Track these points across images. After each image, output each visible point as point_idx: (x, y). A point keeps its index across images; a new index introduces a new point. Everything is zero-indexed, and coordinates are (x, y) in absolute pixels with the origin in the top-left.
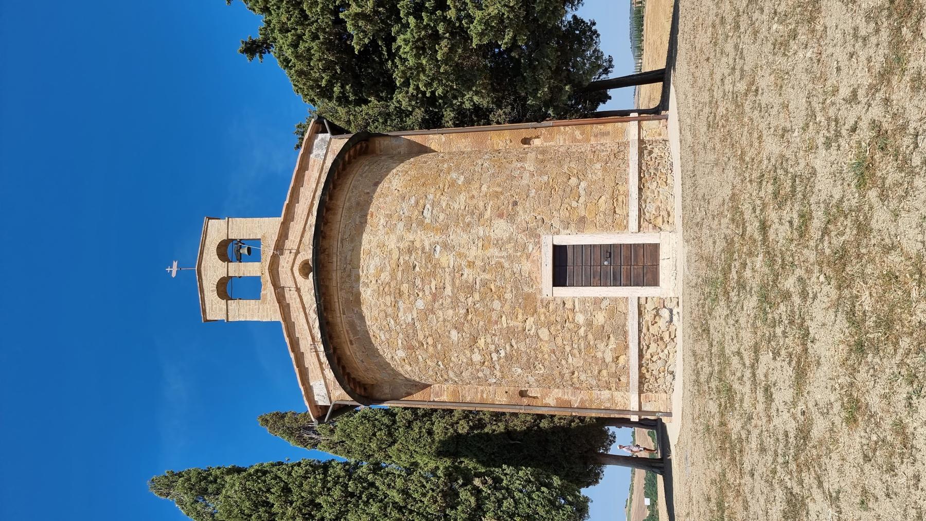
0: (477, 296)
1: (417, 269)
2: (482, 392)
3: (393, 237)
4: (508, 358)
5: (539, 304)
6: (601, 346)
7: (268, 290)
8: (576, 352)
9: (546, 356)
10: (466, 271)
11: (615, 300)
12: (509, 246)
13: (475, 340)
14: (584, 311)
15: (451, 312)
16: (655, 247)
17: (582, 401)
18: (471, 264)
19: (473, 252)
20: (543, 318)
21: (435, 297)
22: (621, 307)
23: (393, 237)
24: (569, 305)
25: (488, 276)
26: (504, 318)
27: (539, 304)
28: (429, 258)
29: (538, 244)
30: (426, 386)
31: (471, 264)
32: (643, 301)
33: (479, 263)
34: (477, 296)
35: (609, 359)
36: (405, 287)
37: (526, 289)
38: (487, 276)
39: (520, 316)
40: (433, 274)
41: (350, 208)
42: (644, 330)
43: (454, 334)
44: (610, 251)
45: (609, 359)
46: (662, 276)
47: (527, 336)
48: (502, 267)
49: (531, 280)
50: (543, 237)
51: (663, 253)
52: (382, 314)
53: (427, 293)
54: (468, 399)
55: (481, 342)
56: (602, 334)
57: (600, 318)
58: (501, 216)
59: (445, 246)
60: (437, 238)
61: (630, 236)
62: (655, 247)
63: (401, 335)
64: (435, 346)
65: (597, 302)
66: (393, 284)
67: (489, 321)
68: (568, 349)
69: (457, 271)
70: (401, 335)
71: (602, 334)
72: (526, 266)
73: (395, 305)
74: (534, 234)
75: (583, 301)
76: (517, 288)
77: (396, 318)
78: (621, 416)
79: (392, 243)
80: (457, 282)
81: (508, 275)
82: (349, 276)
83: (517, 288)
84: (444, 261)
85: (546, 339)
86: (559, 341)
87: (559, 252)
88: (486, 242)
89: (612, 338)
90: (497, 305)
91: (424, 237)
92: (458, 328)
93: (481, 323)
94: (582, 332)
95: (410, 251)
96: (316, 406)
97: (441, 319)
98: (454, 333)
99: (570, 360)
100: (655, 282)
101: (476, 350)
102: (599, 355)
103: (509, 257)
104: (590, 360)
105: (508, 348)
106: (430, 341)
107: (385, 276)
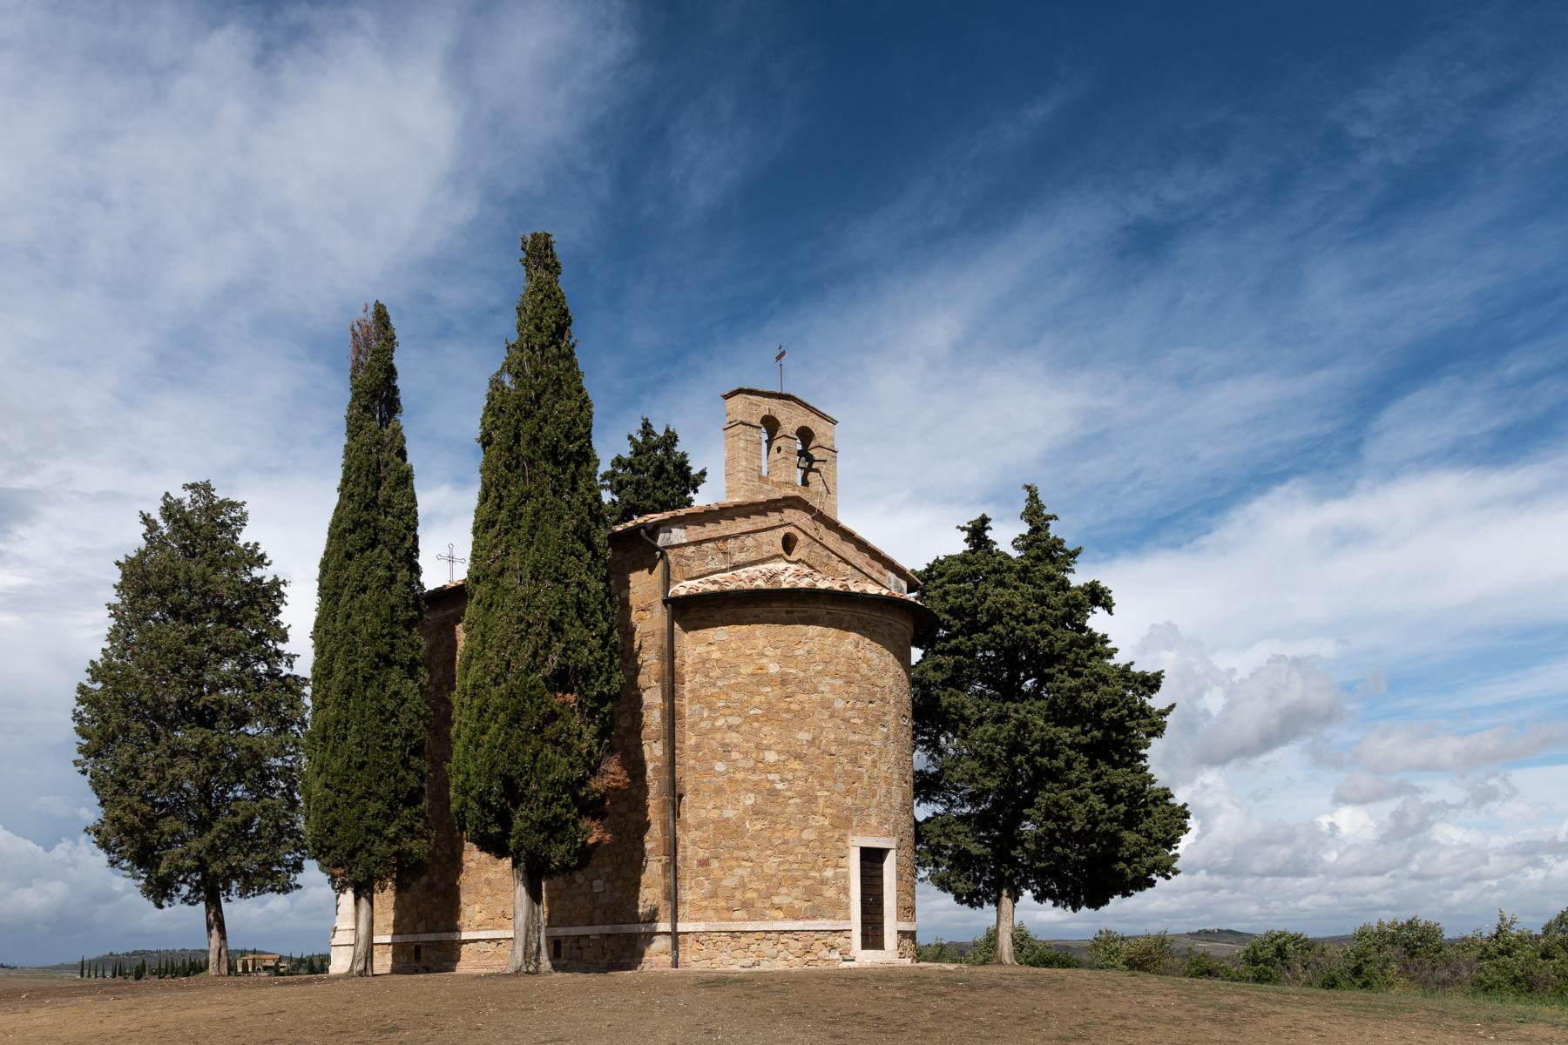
0: (848, 767)
4: (773, 793)
6: (797, 892)
11: (847, 908)
14: (836, 877)
21: (846, 720)
22: (841, 914)
24: (842, 862)
31: (874, 762)
34: (848, 767)
35: (776, 900)
36: (855, 689)
40: (866, 723)
43: (804, 736)
49: (864, 828)
55: (795, 765)
57: (830, 893)
64: (788, 711)
65: (845, 890)
67: (823, 777)
71: (811, 893)
73: (836, 675)
75: (846, 877)
86: (803, 849)
90: (841, 787)
92: (812, 743)
94: (813, 874)
100: (864, 947)
102: (784, 890)
103: (880, 804)
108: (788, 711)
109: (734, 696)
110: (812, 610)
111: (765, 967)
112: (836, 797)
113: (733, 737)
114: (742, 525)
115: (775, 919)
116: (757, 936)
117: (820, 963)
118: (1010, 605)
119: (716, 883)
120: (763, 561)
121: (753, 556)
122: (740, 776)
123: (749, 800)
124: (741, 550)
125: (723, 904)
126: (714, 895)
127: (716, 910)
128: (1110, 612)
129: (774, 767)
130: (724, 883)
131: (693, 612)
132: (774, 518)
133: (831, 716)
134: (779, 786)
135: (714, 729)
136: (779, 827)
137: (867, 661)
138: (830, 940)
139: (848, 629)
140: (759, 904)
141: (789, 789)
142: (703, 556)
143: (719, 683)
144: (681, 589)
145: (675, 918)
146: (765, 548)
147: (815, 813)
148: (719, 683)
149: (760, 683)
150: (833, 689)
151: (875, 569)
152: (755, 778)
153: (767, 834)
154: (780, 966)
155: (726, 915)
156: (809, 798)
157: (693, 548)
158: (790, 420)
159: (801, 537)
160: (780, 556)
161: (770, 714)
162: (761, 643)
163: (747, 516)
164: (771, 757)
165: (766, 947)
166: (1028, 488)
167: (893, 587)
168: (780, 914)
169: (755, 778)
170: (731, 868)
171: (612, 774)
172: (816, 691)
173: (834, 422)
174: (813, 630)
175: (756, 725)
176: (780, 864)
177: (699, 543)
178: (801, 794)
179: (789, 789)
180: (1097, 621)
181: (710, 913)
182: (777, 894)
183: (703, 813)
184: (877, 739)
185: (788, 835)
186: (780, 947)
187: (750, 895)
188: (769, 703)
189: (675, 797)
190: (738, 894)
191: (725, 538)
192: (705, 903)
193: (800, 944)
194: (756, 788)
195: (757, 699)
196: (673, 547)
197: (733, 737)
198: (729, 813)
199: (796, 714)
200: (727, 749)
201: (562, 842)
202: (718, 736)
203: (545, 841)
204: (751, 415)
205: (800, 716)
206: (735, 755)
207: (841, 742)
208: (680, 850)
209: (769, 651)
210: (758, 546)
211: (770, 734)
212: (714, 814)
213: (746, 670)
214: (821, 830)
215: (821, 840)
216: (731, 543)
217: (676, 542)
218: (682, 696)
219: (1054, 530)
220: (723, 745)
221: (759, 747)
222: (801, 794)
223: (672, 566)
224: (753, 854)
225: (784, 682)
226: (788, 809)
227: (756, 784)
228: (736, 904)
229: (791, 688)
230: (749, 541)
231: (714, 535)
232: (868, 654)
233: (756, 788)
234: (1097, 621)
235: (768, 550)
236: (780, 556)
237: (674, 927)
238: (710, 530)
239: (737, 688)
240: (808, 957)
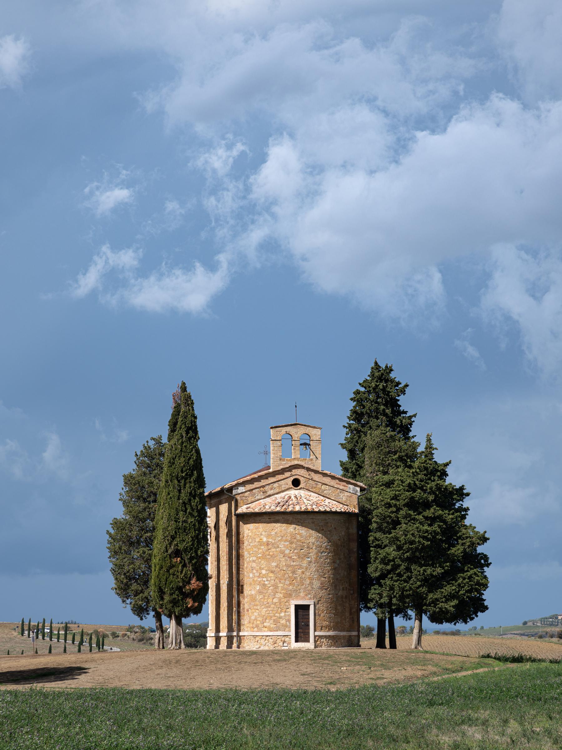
0: (291, 575)
4: (264, 585)
6: (272, 621)
11: (290, 627)
13: (272, 572)
15: (284, 564)
16: (309, 641)
22: (287, 629)
24: (288, 610)
29: (311, 599)
30: (301, 444)
31: (303, 573)
32: (289, 637)
34: (291, 575)
35: (265, 624)
40: (299, 558)
41: (326, 520)
43: (274, 564)
45: (265, 624)
46: (299, 643)
49: (297, 597)
53: (292, 555)
57: (283, 622)
62: (309, 641)
63: (273, 541)
64: (269, 555)
65: (289, 621)
66: (295, 540)
68: (269, 609)
70: (273, 541)
71: (276, 622)
72: (302, 594)
73: (286, 541)
75: (289, 616)
78: (211, 531)
82: (298, 522)
83: (294, 591)
86: (273, 606)
87: (307, 607)
91: (314, 553)
92: (276, 566)
94: (276, 615)
100: (297, 641)
101: (267, 572)
102: (267, 621)
103: (306, 588)
105: (269, 585)
108: (269, 555)
110: (277, 517)
111: (262, 648)
112: (286, 586)
113: (254, 565)
114: (271, 480)
115: (265, 631)
117: (279, 647)
120: (283, 491)
121: (277, 491)
122: (255, 579)
123: (258, 588)
124: (271, 489)
129: (265, 576)
132: (287, 474)
133: (284, 556)
134: (266, 583)
136: (266, 598)
137: (300, 534)
139: (291, 524)
141: (269, 584)
145: (239, 630)
146: (283, 486)
149: (261, 545)
150: (285, 547)
152: (259, 580)
153: (262, 600)
154: (266, 648)
155: (252, 629)
156: (276, 587)
157: (249, 493)
159: (301, 479)
160: (291, 488)
161: (264, 557)
162: (261, 530)
163: (267, 478)
164: (264, 572)
165: (262, 641)
168: (266, 629)
169: (259, 580)
170: (253, 613)
171: (194, 584)
172: (278, 547)
174: (278, 525)
175: (260, 560)
177: (251, 490)
178: (273, 586)
179: (269, 584)
184: (305, 564)
186: (266, 641)
187: (258, 622)
190: (255, 622)
191: (263, 487)
193: (272, 640)
195: (260, 551)
196: (239, 494)
197: (254, 565)
198: (253, 592)
200: (253, 569)
201: (179, 607)
203: (173, 607)
204: (277, 436)
206: (254, 571)
207: (288, 566)
208: (241, 605)
209: (264, 533)
210: (280, 486)
211: (263, 563)
213: (257, 540)
214: (280, 599)
216: (267, 487)
217: (240, 492)
218: (243, 549)
220: (252, 567)
222: (273, 586)
223: (239, 501)
224: (259, 607)
225: (268, 545)
228: (254, 626)
230: (276, 485)
231: (257, 486)
232: (301, 532)
236: (291, 488)
238: (256, 484)
239: (255, 546)
240: (276, 645)
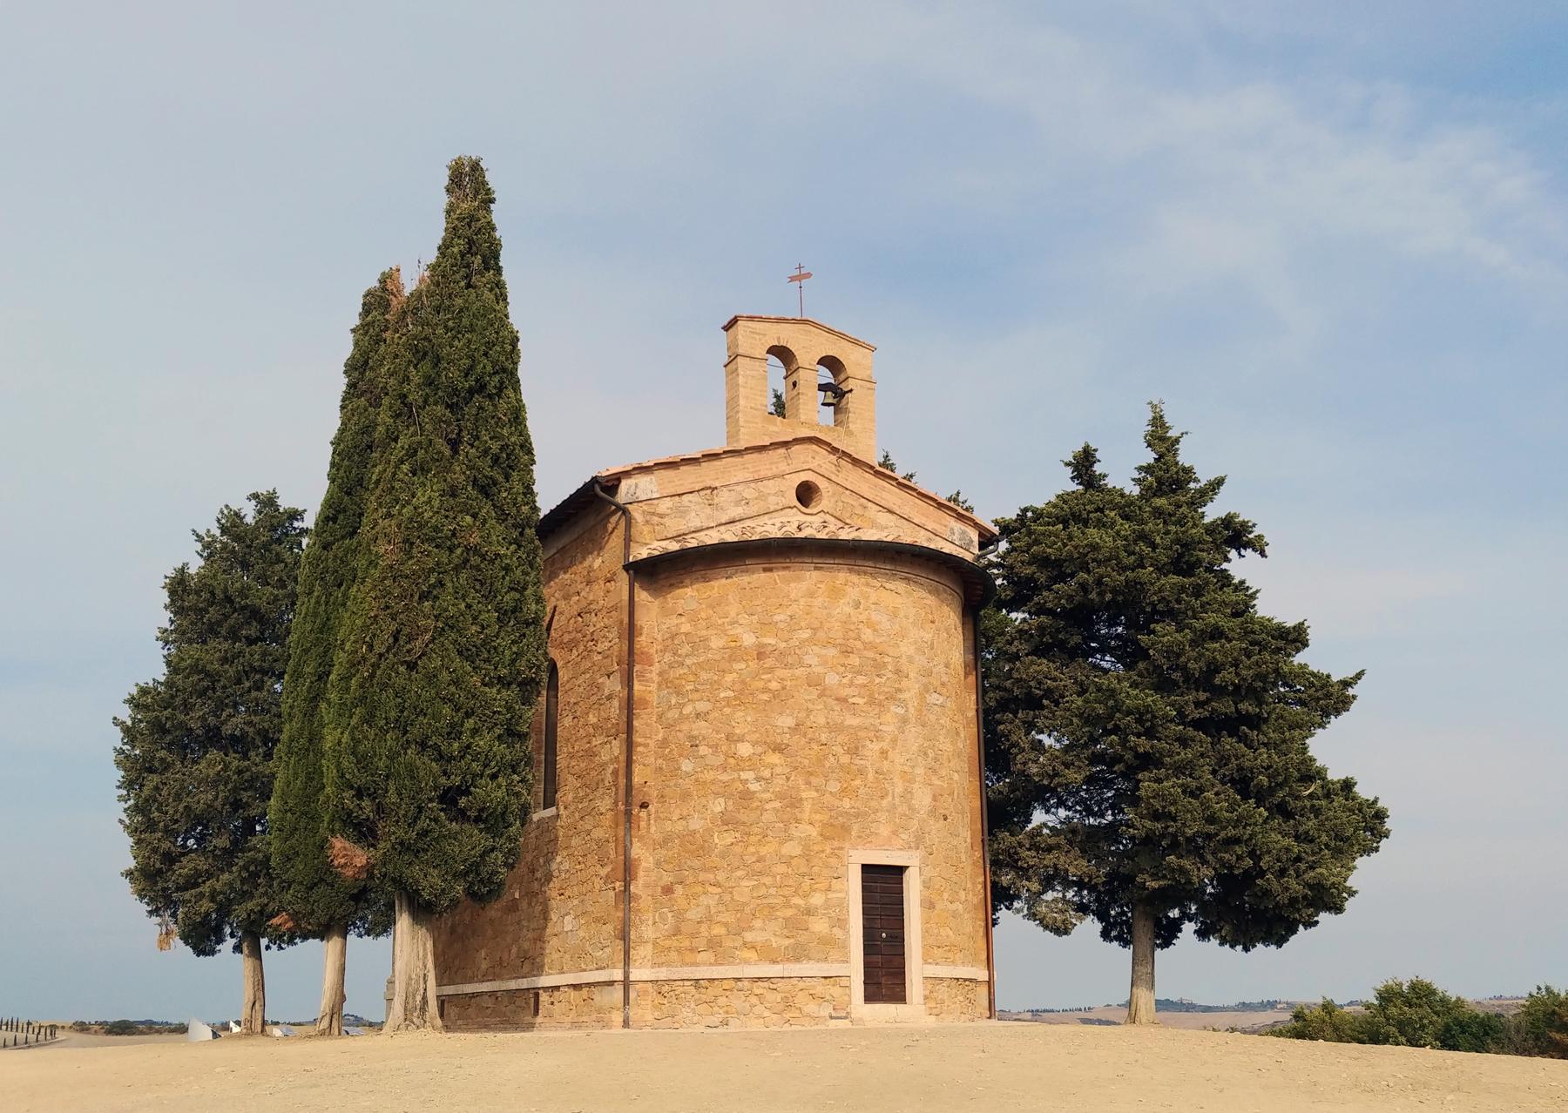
1: (878, 680)
2: (646, 746)
3: (911, 651)
4: (747, 796)
5: (836, 844)
7: (781, 430)
8: (763, 891)
9: (751, 849)
10: (876, 746)
12: (905, 807)
13: (778, 749)
14: (827, 905)
15: (822, 721)
17: (638, 897)
18: (884, 753)
19: (898, 758)
20: (816, 848)
21: (842, 700)
23: (911, 651)
24: (836, 884)
25: (871, 776)
26: (814, 794)
27: (836, 844)
28: (891, 698)
31: (884, 753)
32: (844, 982)
33: (886, 765)
34: (845, 759)
35: (749, 936)
36: (854, 660)
37: (856, 827)
38: (871, 776)
39: (818, 817)
40: (871, 702)
42: (801, 985)
43: (787, 721)
44: (898, 939)
47: (787, 824)
48: (882, 797)
49: (866, 838)
50: (918, 853)
51: (900, 1006)
52: (816, 624)
54: (636, 723)
55: (775, 758)
56: (795, 925)
57: (819, 926)
58: (935, 799)
59: (904, 721)
60: (912, 710)
61: (916, 968)
64: (765, 690)
65: (841, 923)
66: (858, 644)
68: (767, 880)
69: (878, 735)
71: (795, 925)
73: (829, 643)
74: (918, 842)
76: (857, 816)
77: (812, 641)
79: (906, 649)
80: (862, 734)
81: (873, 804)
83: (857, 816)
84: (888, 717)
85: (784, 851)
86: (782, 869)
88: (908, 778)
89: (787, 942)
90: (834, 786)
91: (913, 692)
92: (796, 728)
93: (806, 762)
95: (898, 672)
96: (619, 480)
97: (810, 706)
98: (789, 721)
99: (745, 883)
100: (869, 998)
101: (759, 750)
102: (758, 924)
104: (747, 910)
106: (774, 685)
107: (867, 635)
108: (765, 690)
109: (704, 676)
113: (700, 728)
115: (747, 962)
116: (726, 985)
118: (1095, 547)
119: (680, 916)
122: (709, 776)
123: (718, 806)
125: (687, 943)
126: (677, 932)
127: (679, 951)
128: (1263, 554)
129: (752, 763)
130: (689, 915)
131: (659, 572)
134: (754, 787)
135: (683, 718)
136: (753, 839)
138: (819, 989)
140: (728, 943)
142: (682, 512)
143: (688, 662)
144: (641, 553)
147: (798, 821)
148: (688, 662)
151: (884, 518)
152: (725, 777)
153: (738, 849)
155: (689, 957)
158: (808, 348)
159: (822, 484)
166: (1154, 407)
167: (957, 541)
169: (725, 777)
173: (873, 349)
175: (727, 710)
176: (754, 888)
178: (780, 796)
180: (1240, 566)
181: (674, 955)
182: (751, 928)
183: (668, 826)
185: (763, 851)
187: (718, 930)
188: (743, 682)
189: (630, 803)
192: (668, 943)
194: (724, 791)
195: (729, 678)
197: (700, 728)
198: (696, 824)
199: (775, 695)
202: (685, 727)
205: (780, 697)
206: (703, 750)
209: (744, 619)
210: (762, 497)
212: (680, 826)
214: (806, 844)
215: (807, 856)
219: (1184, 458)
221: (731, 738)
222: (780, 796)
224: (721, 876)
226: (765, 817)
227: (726, 785)
228: (701, 943)
229: (769, 662)
233: (724, 791)
234: (1240, 566)
235: (773, 502)
237: (626, 975)
